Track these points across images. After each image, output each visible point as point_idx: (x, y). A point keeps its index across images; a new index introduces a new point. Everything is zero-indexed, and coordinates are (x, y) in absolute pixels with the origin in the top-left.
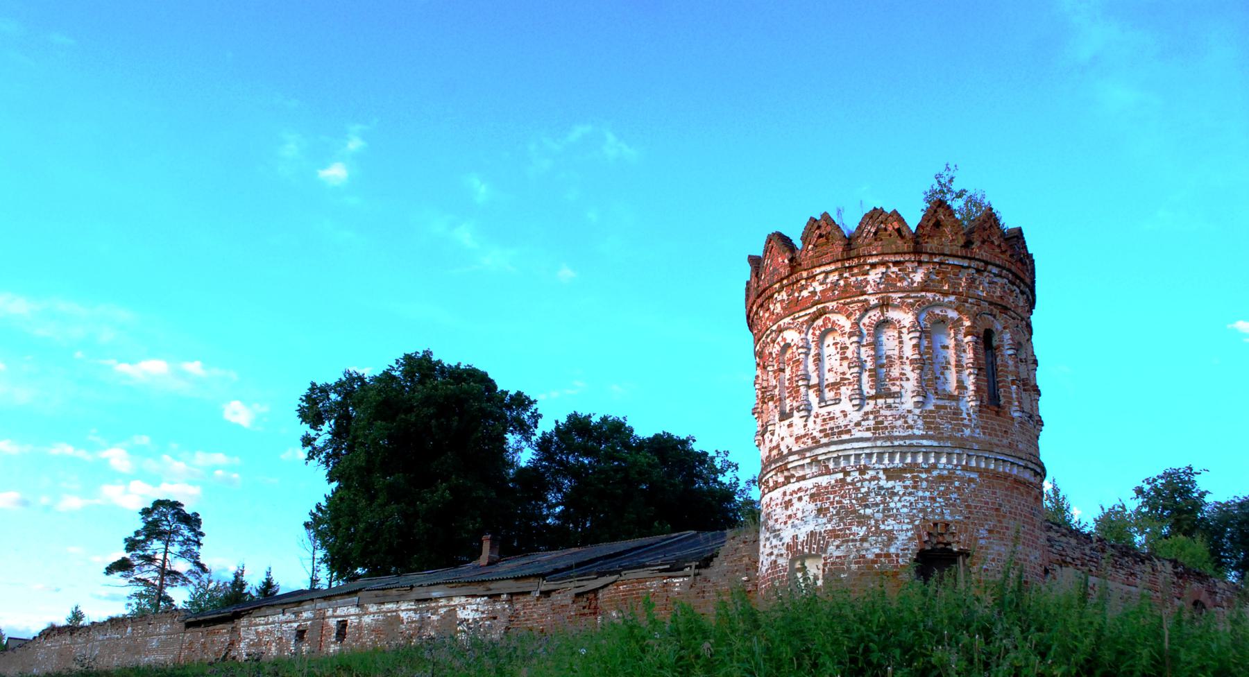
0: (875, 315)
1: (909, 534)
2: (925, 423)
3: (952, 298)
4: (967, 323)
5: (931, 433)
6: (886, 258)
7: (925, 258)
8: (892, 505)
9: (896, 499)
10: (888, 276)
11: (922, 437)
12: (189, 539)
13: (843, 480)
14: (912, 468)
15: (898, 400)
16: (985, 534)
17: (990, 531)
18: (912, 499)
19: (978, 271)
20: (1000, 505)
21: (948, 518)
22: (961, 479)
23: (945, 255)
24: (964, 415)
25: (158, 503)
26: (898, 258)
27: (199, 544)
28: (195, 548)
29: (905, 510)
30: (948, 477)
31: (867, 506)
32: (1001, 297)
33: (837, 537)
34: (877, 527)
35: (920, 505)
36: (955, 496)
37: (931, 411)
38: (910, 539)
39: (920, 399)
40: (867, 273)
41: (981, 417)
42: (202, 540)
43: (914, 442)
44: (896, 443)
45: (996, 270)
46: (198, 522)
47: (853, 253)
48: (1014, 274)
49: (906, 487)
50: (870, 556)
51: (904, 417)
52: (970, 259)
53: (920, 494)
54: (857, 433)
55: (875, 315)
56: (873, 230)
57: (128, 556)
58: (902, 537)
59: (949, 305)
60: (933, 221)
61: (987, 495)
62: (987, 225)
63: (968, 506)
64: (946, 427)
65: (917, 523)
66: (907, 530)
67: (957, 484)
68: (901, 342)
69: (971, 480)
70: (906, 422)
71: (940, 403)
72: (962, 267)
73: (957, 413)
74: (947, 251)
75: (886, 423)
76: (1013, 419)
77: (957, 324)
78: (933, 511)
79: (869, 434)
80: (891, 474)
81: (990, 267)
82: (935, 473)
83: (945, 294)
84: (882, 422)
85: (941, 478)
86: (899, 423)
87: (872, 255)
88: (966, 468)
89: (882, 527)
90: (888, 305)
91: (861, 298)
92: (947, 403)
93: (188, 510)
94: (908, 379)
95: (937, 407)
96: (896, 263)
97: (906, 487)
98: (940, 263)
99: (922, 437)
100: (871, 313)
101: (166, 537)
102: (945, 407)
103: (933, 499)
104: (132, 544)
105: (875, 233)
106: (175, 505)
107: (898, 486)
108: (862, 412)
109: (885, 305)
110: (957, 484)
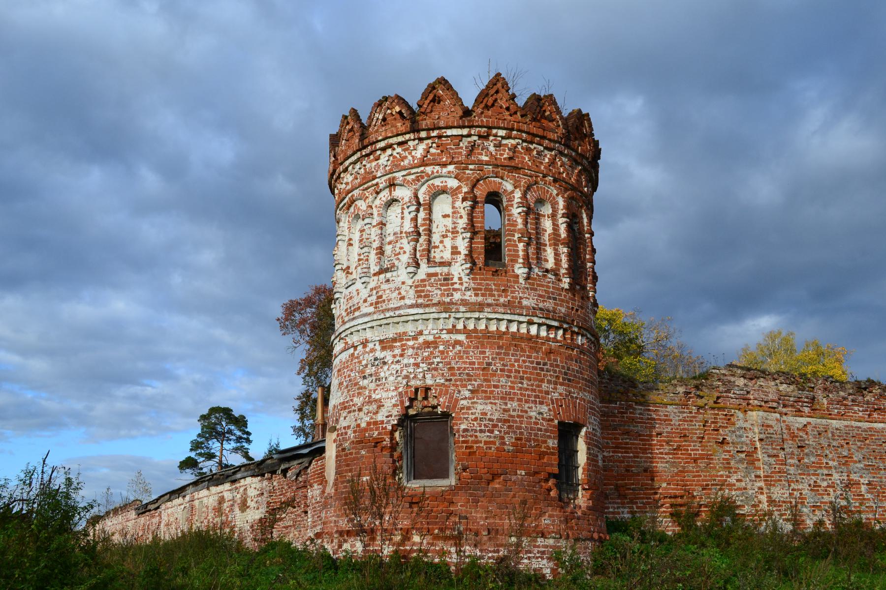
0: (385, 195)
1: (393, 401)
2: (417, 292)
3: (451, 168)
4: (465, 189)
5: (420, 301)
6: (391, 141)
7: (423, 134)
8: (382, 375)
9: (386, 368)
10: (395, 157)
11: (412, 306)
12: (241, 438)
13: (353, 354)
14: (399, 338)
15: (394, 274)
16: (467, 394)
17: (472, 392)
18: (398, 367)
19: (480, 137)
20: (489, 364)
21: (429, 382)
22: (446, 343)
23: (440, 128)
24: (456, 280)
25: (213, 410)
26: (400, 139)
27: (248, 441)
28: (246, 445)
29: (391, 378)
30: (434, 342)
31: (365, 378)
32: (510, 158)
33: (345, 408)
34: (370, 397)
35: (405, 373)
36: (438, 360)
37: (423, 281)
38: (394, 405)
39: (411, 269)
40: (378, 159)
41: (473, 279)
42: (251, 438)
43: (402, 312)
44: (388, 315)
45: (502, 133)
46: (245, 424)
47: (366, 142)
48: (528, 133)
49: (394, 356)
50: (363, 425)
51: (399, 289)
52: (470, 127)
53: (406, 361)
54: (365, 309)
55: (385, 195)
56: (381, 117)
57: (193, 455)
58: (388, 404)
59: (449, 175)
60: (431, 97)
61: (474, 356)
62: (492, 92)
63: (451, 369)
64: (436, 295)
65: (400, 390)
66: (392, 398)
67: (441, 348)
68: (402, 218)
69: (458, 342)
70: (400, 294)
71: (432, 270)
72: (462, 136)
73: (447, 278)
74: (442, 124)
75: (384, 297)
76: (517, 276)
77: (454, 192)
78: (415, 377)
79: (372, 309)
80: (385, 344)
81: (494, 131)
82: (421, 339)
83: (444, 165)
84: (381, 297)
85: (427, 344)
86: (395, 294)
87: (378, 141)
88: (453, 330)
89: (373, 396)
90: (394, 185)
91: (374, 182)
92: (438, 270)
93: (236, 413)
94: (405, 252)
95: (430, 275)
96: (400, 144)
97: (394, 356)
98: (440, 137)
99: (412, 306)
100: (381, 195)
101: (221, 436)
102: (436, 274)
103: (417, 365)
104: (196, 446)
105: (384, 119)
106: (227, 412)
107: (388, 355)
108: (368, 289)
109: (392, 185)
110: (441, 348)
